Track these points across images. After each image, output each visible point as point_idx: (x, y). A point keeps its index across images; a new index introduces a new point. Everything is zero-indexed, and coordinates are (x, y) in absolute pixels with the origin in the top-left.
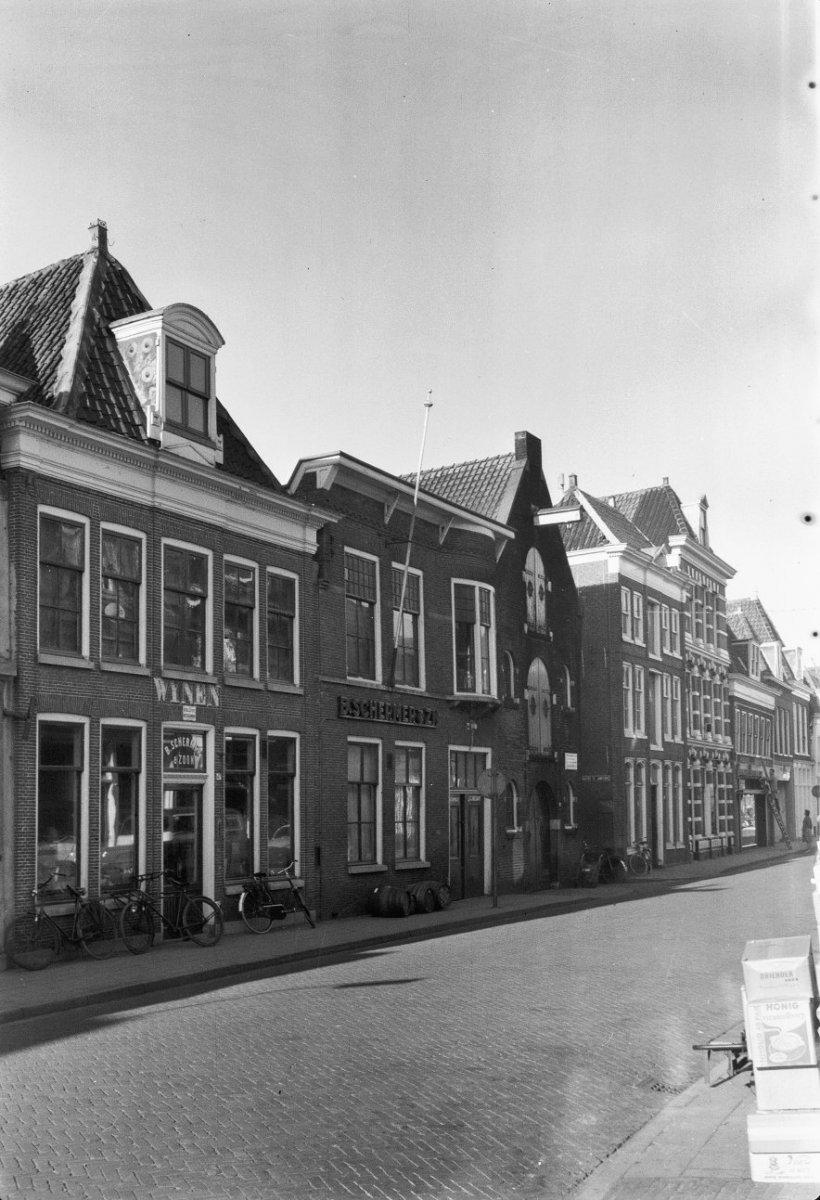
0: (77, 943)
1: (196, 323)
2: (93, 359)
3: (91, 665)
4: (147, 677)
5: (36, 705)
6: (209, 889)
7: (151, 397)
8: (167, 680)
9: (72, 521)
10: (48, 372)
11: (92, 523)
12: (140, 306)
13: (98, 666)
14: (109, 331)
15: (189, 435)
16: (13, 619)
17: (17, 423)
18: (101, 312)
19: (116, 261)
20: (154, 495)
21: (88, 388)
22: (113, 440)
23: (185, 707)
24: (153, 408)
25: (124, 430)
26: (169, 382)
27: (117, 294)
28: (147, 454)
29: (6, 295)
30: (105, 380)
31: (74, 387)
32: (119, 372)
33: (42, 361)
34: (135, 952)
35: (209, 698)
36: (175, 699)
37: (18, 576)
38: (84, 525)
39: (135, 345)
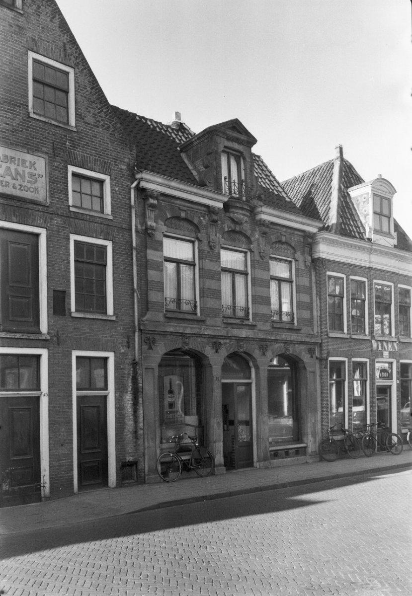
0: (346, 451)
1: (386, 186)
2: (343, 206)
3: (348, 336)
4: (369, 340)
5: (328, 356)
6: (395, 430)
7: (367, 220)
8: (377, 341)
9: (339, 277)
10: (325, 214)
11: (347, 277)
12: (358, 180)
13: (350, 336)
14: (347, 193)
15: (383, 234)
16: (318, 319)
17: (319, 240)
18: (344, 185)
19: (347, 161)
20: (370, 262)
21: (343, 220)
22: (356, 242)
23: (384, 352)
24: (368, 224)
25: (357, 236)
26: (375, 213)
27: (350, 177)
28: (368, 245)
29: (299, 180)
30: (348, 215)
31: (338, 220)
32: (353, 210)
33: (321, 210)
34: (368, 456)
35: (393, 347)
36: (380, 349)
37: (320, 301)
38: (343, 278)
39: (359, 198)
